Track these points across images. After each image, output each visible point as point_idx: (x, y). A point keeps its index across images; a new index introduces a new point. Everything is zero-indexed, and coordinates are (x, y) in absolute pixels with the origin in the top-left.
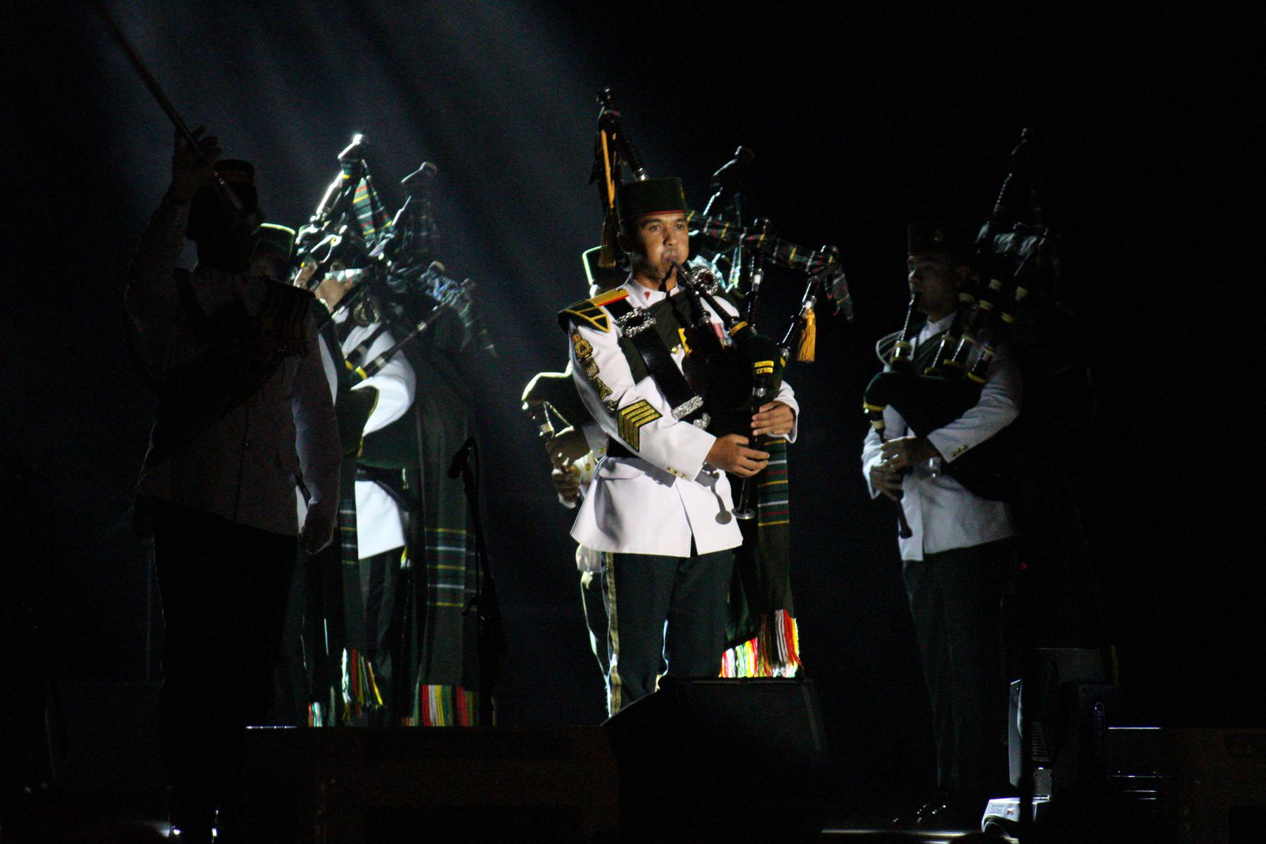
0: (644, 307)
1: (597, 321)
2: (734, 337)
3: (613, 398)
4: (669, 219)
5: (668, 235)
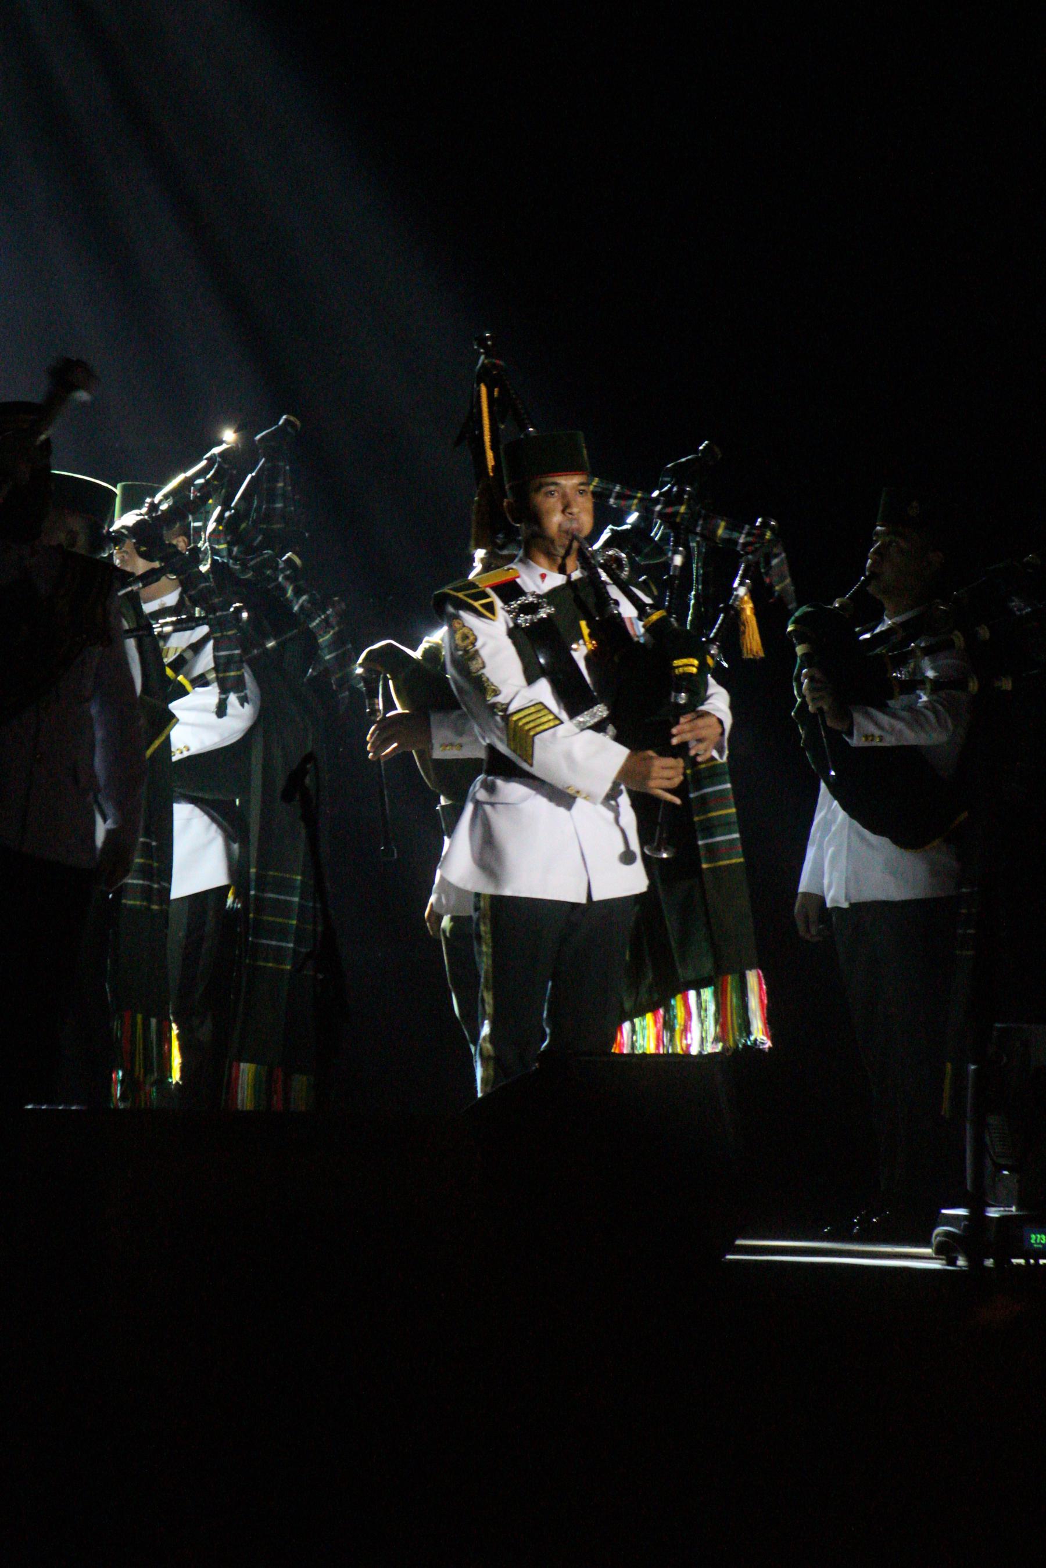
0: (539, 592)
1: (483, 605)
2: (649, 629)
3: (500, 699)
4: (570, 482)
5: (568, 502)
